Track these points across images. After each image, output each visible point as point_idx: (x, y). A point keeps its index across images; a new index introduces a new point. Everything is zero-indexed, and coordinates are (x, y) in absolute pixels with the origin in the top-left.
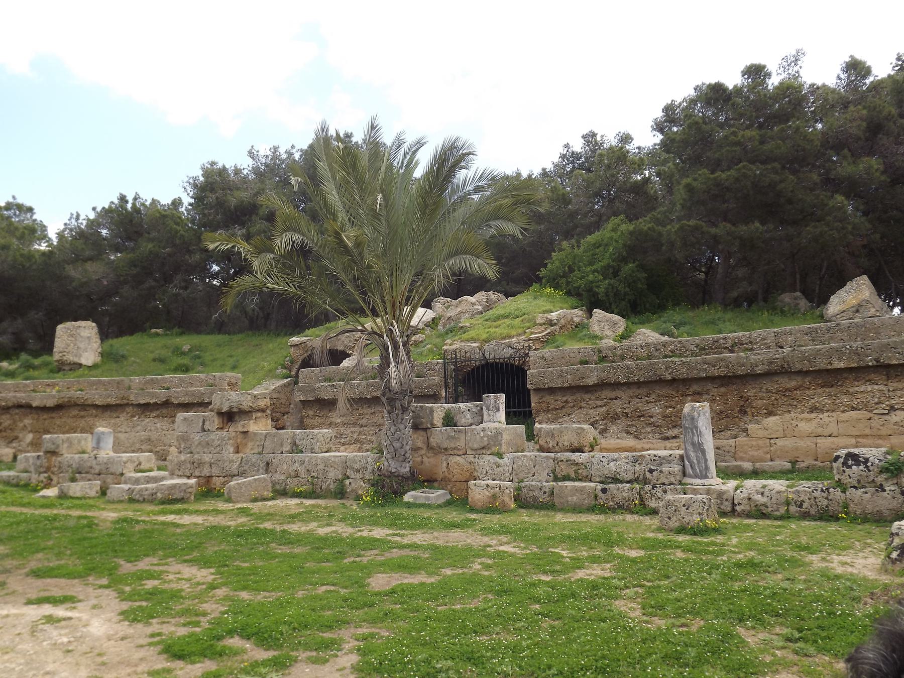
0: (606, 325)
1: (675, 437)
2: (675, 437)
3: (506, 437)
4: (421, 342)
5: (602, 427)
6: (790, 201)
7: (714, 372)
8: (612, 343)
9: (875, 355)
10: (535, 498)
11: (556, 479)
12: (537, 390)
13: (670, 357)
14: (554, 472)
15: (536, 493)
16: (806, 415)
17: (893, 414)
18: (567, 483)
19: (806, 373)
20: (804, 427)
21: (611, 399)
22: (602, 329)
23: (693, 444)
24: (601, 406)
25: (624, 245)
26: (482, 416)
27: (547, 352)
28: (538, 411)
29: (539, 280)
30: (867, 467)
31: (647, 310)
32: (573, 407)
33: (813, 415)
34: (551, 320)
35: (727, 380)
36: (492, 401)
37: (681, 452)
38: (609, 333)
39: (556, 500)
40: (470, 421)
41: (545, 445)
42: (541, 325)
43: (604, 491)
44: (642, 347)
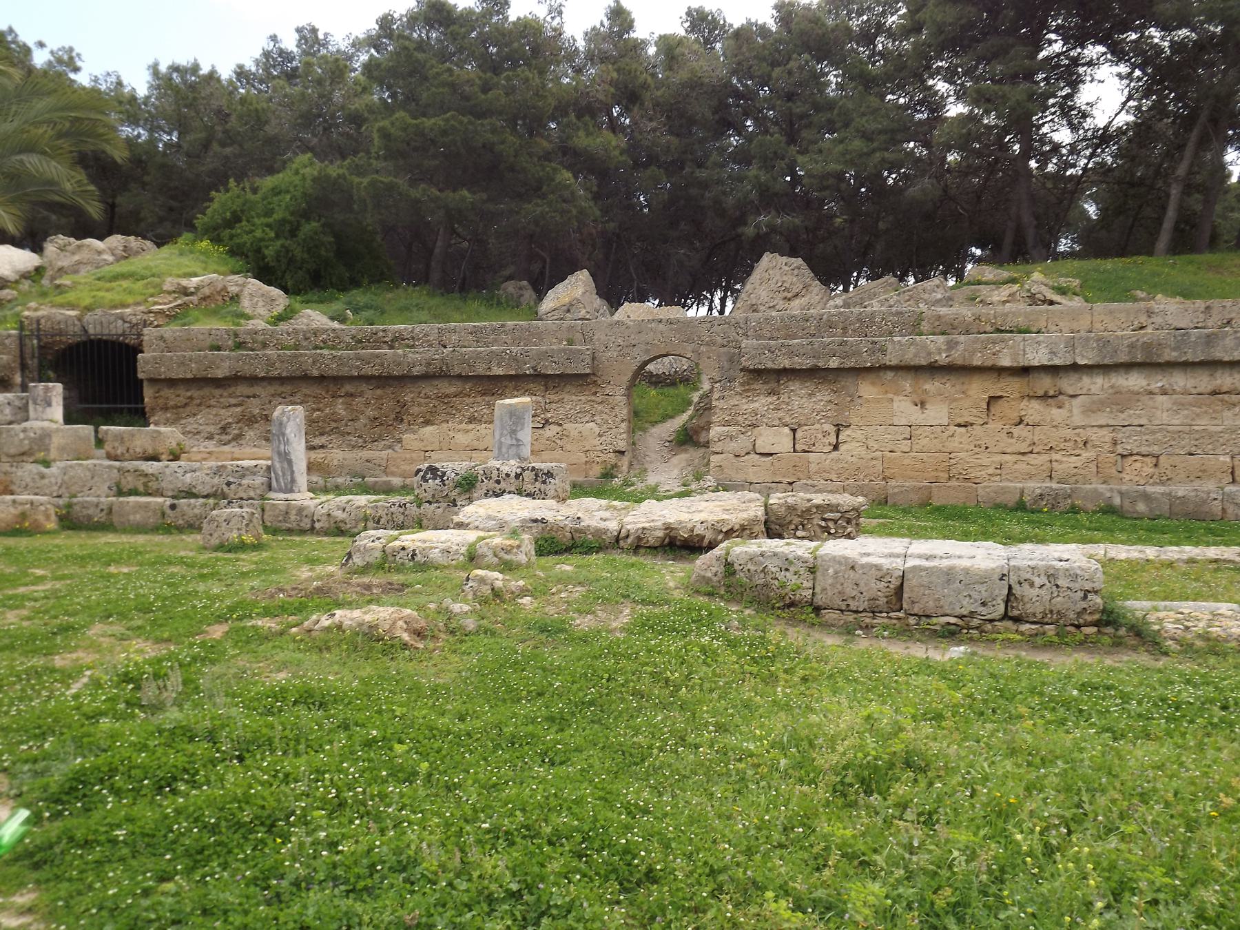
0: (260, 300)
1: (322, 447)
2: (322, 447)
3: (56, 441)
4: (9, 301)
5: (236, 432)
6: (512, 169)
7: (368, 370)
8: (259, 324)
9: (533, 363)
10: (90, 517)
11: (120, 493)
12: (153, 381)
13: (321, 348)
14: (118, 485)
15: (90, 512)
16: (464, 425)
17: (547, 428)
18: (132, 499)
19: (467, 378)
20: (462, 439)
21: (248, 397)
22: (254, 306)
23: (279, 453)
24: (235, 405)
25: (305, 194)
26: (27, 411)
27: (171, 331)
28: (153, 409)
29: (191, 227)
30: (443, 481)
31: (332, 285)
32: (200, 405)
33: (471, 426)
34: (185, 288)
35: (383, 380)
36: (41, 393)
37: (269, 463)
38: (261, 310)
39: (115, 519)
40: (9, 418)
41: (112, 452)
42: (169, 293)
43: (173, 507)
44: (289, 334)
